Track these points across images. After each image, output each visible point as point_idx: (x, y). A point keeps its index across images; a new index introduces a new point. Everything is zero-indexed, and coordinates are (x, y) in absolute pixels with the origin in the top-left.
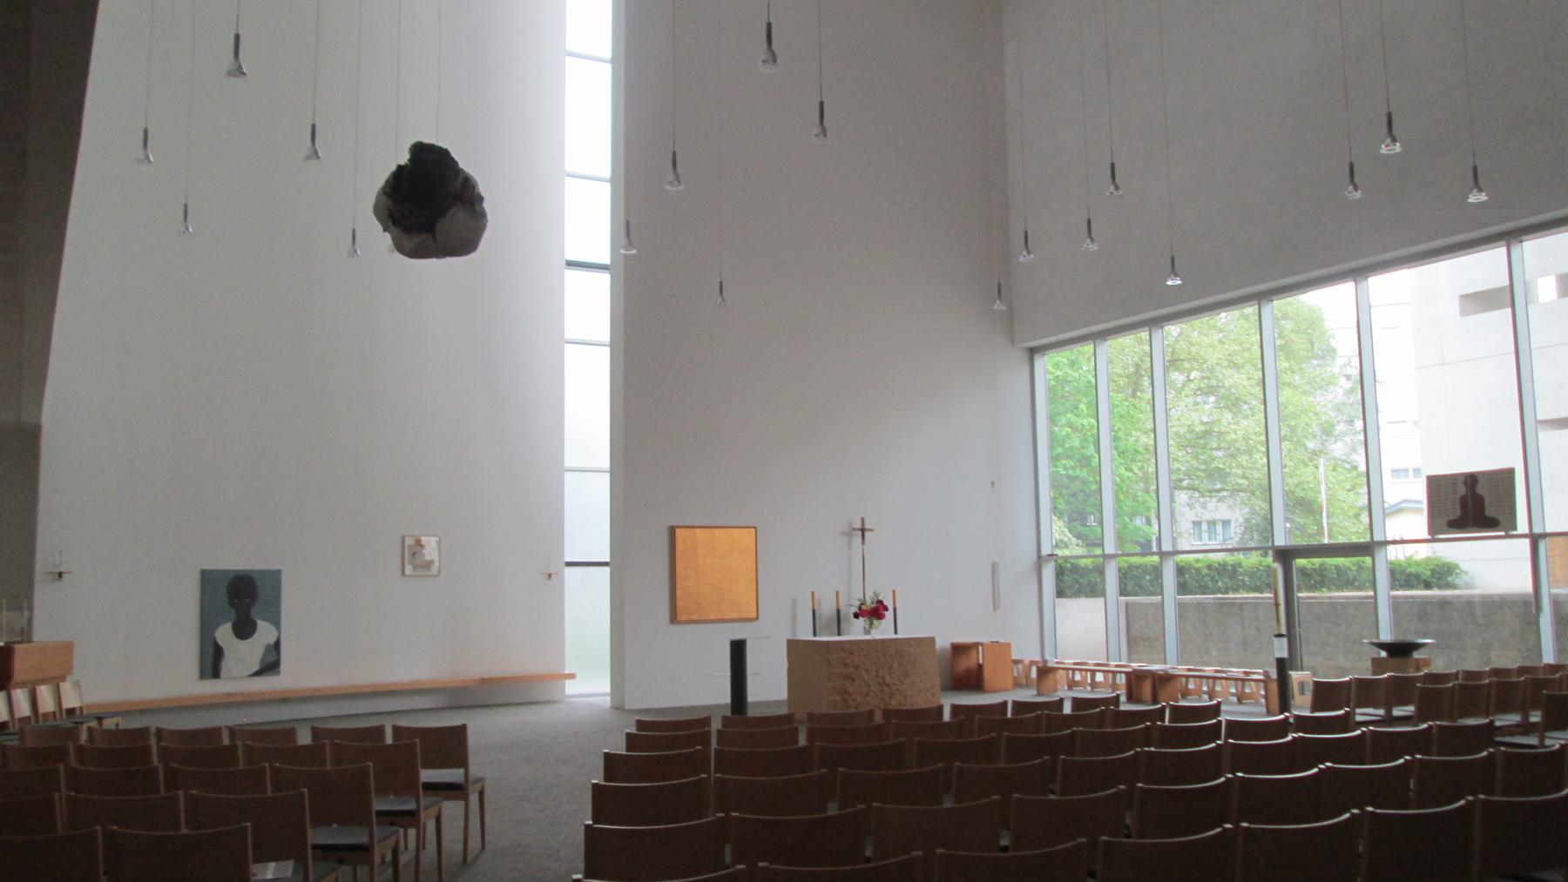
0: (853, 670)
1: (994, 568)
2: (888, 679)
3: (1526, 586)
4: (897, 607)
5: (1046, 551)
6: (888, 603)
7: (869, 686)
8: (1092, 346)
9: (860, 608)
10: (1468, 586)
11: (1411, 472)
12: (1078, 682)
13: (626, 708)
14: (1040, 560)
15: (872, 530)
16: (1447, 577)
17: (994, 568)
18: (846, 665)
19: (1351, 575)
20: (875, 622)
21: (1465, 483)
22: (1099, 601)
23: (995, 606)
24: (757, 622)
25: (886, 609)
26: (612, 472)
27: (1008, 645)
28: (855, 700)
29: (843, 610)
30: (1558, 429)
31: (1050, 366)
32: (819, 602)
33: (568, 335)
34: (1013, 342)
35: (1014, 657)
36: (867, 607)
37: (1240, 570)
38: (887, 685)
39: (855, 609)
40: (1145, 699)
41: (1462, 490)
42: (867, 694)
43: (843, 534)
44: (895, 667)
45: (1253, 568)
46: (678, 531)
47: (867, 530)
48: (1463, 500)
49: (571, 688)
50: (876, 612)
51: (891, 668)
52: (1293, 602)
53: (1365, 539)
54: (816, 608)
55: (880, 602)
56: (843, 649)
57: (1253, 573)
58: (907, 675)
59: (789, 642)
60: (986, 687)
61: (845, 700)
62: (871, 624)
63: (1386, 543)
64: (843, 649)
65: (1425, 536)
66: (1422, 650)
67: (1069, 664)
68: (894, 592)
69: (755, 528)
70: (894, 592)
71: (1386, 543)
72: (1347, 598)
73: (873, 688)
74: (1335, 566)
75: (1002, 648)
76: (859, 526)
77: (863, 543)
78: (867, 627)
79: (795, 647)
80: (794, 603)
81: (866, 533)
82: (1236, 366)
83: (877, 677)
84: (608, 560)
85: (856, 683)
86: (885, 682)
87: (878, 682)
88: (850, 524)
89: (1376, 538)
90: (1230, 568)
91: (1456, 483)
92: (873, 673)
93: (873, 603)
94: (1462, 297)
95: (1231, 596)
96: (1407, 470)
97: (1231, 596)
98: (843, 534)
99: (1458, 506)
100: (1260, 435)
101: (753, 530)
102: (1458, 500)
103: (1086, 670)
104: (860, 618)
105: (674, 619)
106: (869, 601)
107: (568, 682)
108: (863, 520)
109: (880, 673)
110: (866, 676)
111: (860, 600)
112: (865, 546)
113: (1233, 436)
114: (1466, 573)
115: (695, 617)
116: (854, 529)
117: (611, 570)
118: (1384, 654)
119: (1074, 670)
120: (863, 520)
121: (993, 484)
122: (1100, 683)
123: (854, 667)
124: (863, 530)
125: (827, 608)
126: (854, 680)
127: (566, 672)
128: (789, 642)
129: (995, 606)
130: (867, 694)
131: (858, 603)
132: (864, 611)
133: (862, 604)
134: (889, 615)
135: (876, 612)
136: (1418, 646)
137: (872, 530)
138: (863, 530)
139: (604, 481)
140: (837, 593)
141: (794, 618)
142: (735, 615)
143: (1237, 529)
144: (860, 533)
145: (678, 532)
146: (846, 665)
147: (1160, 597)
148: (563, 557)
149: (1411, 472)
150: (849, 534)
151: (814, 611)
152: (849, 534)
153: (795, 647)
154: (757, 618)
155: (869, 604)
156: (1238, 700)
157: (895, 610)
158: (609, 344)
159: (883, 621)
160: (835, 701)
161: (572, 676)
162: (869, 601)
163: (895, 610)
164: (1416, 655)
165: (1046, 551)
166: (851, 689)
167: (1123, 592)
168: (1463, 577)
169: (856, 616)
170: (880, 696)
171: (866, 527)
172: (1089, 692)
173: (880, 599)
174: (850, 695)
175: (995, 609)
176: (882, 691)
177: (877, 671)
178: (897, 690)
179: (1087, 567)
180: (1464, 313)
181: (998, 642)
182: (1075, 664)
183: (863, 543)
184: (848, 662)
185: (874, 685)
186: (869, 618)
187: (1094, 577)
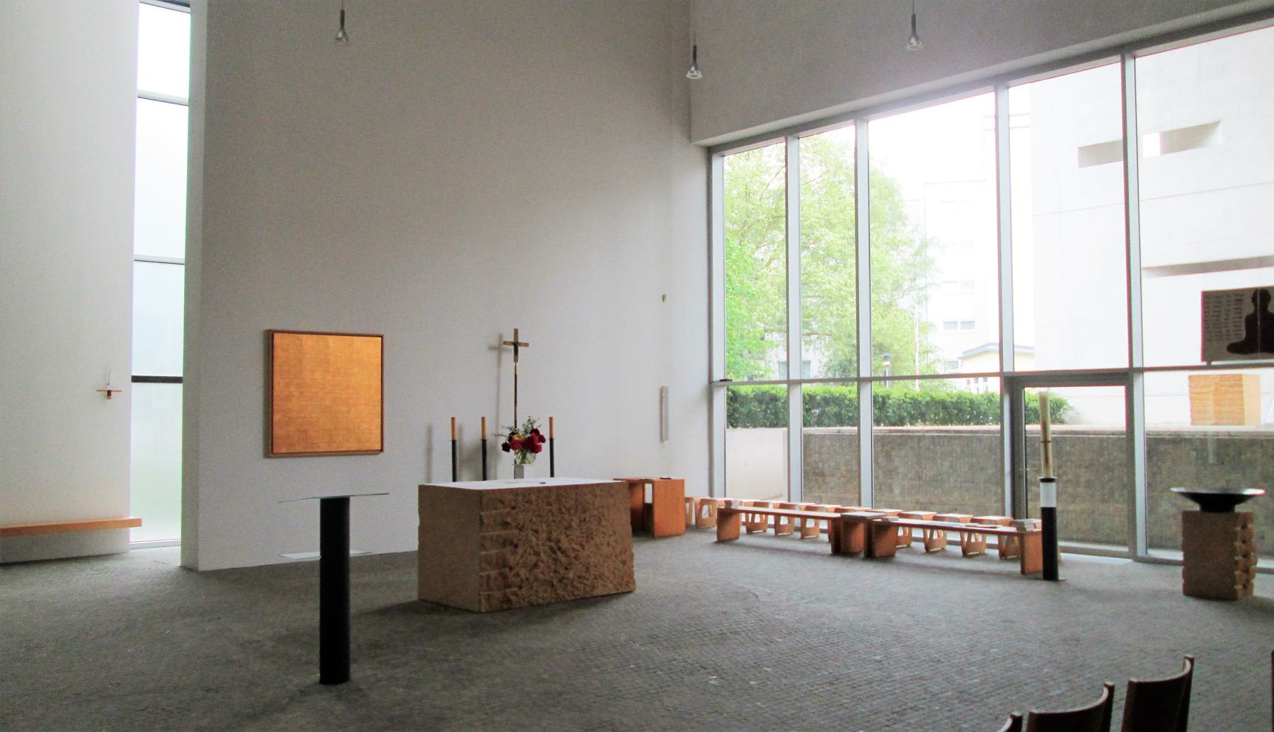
0: (516, 531)
1: (663, 394)
2: (565, 544)
3: (1120, 424)
4: (554, 437)
5: (717, 376)
6: (544, 432)
7: (537, 554)
8: (784, 144)
9: (510, 439)
10: (1074, 422)
11: (959, 324)
12: (758, 524)
13: (201, 568)
14: (711, 386)
15: (526, 345)
16: (921, 419)
17: (663, 394)
18: (506, 525)
19: (983, 409)
20: (529, 455)
21: (1254, 299)
22: (780, 432)
23: (663, 437)
24: (382, 454)
25: (543, 440)
26: (189, 264)
27: (682, 482)
28: (517, 575)
29: (489, 438)
30: (1163, 276)
31: (730, 165)
32: (461, 430)
33: (143, 85)
34: (690, 138)
35: (687, 495)
36: (519, 437)
37: (890, 402)
38: (563, 552)
39: (504, 440)
40: (857, 550)
41: (1248, 309)
42: (536, 565)
43: (492, 348)
44: (574, 525)
45: (899, 400)
46: (277, 336)
47: (521, 344)
48: (1250, 321)
49: (135, 535)
50: (529, 443)
51: (569, 527)
52: (1020, 440)
53: (1123, 364)
54: (457, 438)
55: (536, 431)
56: (502, 502)
57: (900, 405)
58: (589, 536)
59: (422, 489)
60: (656, 533)
61: (504, 576)
62: (524, 457)
63: (1142, 370)
64: (502, 502)
65: (1197, 361)
66: (1249, 502)
67: (747, 504)
68: (551, 419)
69: (382, 337)
70: (551, 419)
71: (1142, 370)
72: (972, 432)
73: (543, 557)
74: (970, 400)
75: (673, 487)
76: (512, 340)
77: (516, 360)
78: (518, 461)
79: (429, 496)
80: (430, 431)
81: (520, 348)
82: (831, 226)
83: (549, 540)
84: (180, 374)
85: (520, 550)
86: (560, 549)
87: (551, 548)
88: (501, 336)
89: (1136, 364)
90: (880, 399)
91: (1240, 300)
92: (544, 535)
93: (526, 431)
94: (1080, 148)
95: (908, 427)
96: (956, 323)
97: (908, 427)
98: (492, 348)
99: (1243, 327)
100: (851, 286)
101: (380, 338)
102: (1243, 319)
103: (767, 514)
104: (511, 450)
105: (270, 450)
106: (520, 428)
107: (132, 530)
108: (516, 332)
109: (554, 535)
110: (534, 539)
111: (511, 429)
112: (517, 363)
113: (828, 286)
114: (1072, 408)
115: (299, 449)
116: (505, 343)
117: (184, 387)
118: (1196, 507)
119: (754, 513)
120: (516, 332)
121: (664, 297)
122: (784, 526)
123: (517, 527)
124: (516, 345)
125: (470, 438)
126: (516, 546)
127: (131, 517)
128: (422, 489)
129: (663, 437)
130: (536, 565)
131: (508, 432)
132: (516, 442)
133: (513, 433)
134: (545, 446)
135: (529, 443)
136: (1243, 499)
137: (526, 345)
138: (516, 345)
139: (178, 276)
140: (483, 419)
141: (429, 450)
142: (354, 447)
143: (821, 369)
144: (512, 347)
145: (278, 339)
146: (506, 525)
147: (856, 428)
148: (131, 373)
149: (959, 324)
150: (498, 348)
151: (454, 442)
152: (498, 348)
153: (429, 496)
154: (382, 450)
155: (522, 434)
156: (927, 548)
157: (551, 440)
158: (187, 101)
159: (539, 455)
160: (488, 577)
161: (137, 523)
162: (520, 428)
163: (551, 440)
164: (1239, 508)
165: (717, 376)
166: (512, 560)
167: (806, 423)
168: (1070, 413)
169: (506, 448)
170: (553, 567)
171: (520, 341)
172: (769, 537)
173: (535, 428)
174: (511, 569)
175: (662, 440)
176: (556, 560)
177: (550, 533)
178: (576, 558)
179: (747, 395)
180: (1082, 164)
181: (670, 479)
182: (756, 504)
183: (516, 360)
184: (509, 520)
185: (545, 552)
186: (522, 451)
187: (754, 406)
